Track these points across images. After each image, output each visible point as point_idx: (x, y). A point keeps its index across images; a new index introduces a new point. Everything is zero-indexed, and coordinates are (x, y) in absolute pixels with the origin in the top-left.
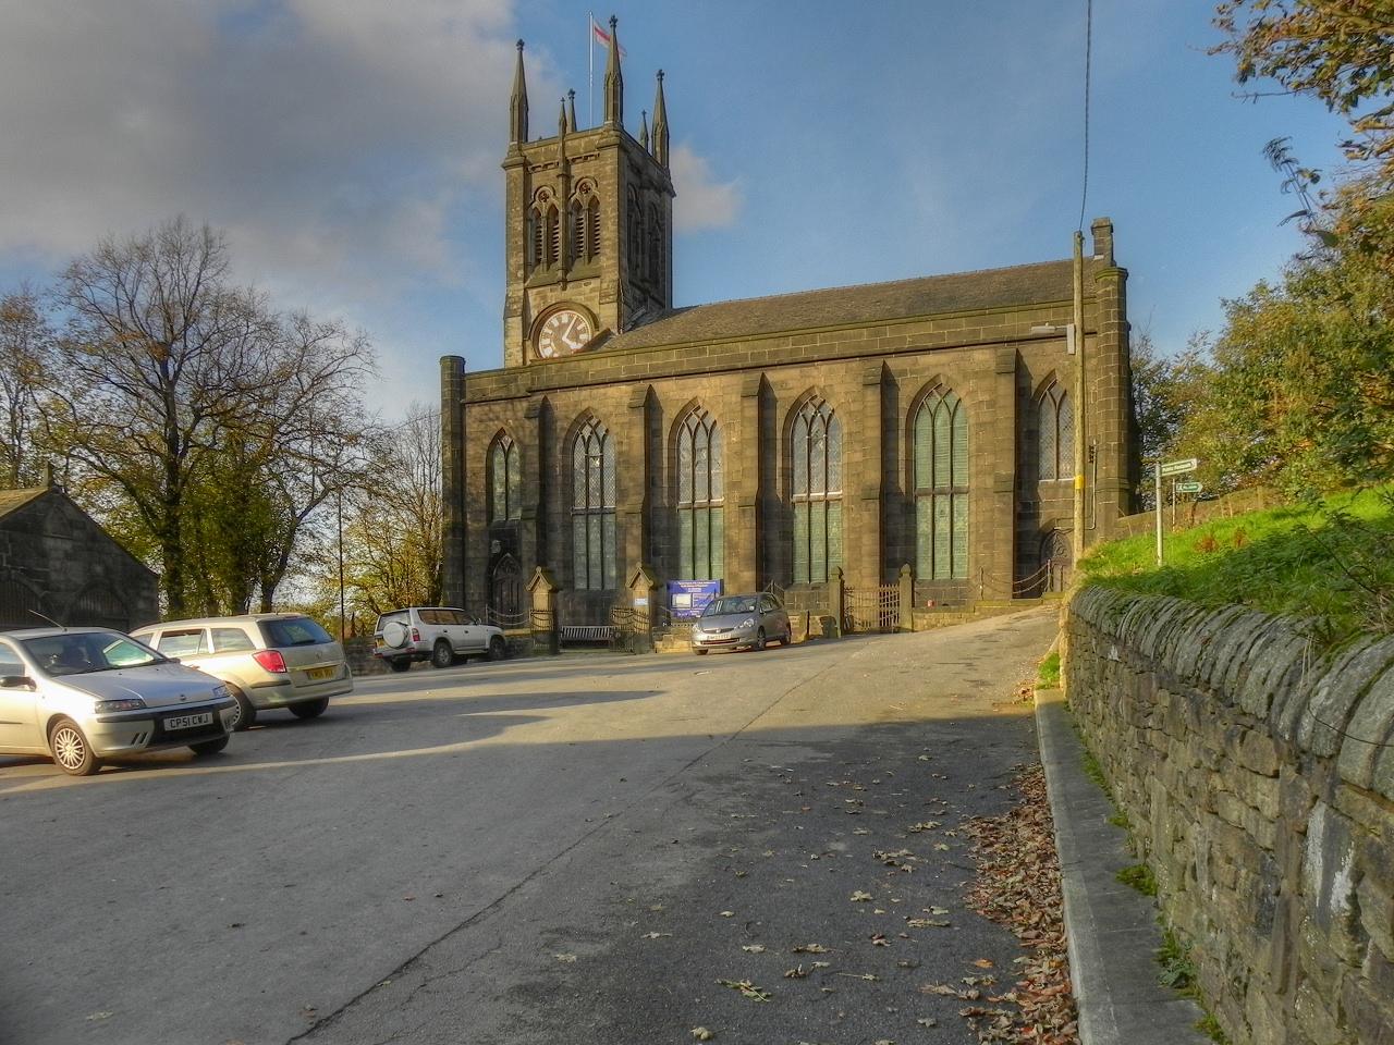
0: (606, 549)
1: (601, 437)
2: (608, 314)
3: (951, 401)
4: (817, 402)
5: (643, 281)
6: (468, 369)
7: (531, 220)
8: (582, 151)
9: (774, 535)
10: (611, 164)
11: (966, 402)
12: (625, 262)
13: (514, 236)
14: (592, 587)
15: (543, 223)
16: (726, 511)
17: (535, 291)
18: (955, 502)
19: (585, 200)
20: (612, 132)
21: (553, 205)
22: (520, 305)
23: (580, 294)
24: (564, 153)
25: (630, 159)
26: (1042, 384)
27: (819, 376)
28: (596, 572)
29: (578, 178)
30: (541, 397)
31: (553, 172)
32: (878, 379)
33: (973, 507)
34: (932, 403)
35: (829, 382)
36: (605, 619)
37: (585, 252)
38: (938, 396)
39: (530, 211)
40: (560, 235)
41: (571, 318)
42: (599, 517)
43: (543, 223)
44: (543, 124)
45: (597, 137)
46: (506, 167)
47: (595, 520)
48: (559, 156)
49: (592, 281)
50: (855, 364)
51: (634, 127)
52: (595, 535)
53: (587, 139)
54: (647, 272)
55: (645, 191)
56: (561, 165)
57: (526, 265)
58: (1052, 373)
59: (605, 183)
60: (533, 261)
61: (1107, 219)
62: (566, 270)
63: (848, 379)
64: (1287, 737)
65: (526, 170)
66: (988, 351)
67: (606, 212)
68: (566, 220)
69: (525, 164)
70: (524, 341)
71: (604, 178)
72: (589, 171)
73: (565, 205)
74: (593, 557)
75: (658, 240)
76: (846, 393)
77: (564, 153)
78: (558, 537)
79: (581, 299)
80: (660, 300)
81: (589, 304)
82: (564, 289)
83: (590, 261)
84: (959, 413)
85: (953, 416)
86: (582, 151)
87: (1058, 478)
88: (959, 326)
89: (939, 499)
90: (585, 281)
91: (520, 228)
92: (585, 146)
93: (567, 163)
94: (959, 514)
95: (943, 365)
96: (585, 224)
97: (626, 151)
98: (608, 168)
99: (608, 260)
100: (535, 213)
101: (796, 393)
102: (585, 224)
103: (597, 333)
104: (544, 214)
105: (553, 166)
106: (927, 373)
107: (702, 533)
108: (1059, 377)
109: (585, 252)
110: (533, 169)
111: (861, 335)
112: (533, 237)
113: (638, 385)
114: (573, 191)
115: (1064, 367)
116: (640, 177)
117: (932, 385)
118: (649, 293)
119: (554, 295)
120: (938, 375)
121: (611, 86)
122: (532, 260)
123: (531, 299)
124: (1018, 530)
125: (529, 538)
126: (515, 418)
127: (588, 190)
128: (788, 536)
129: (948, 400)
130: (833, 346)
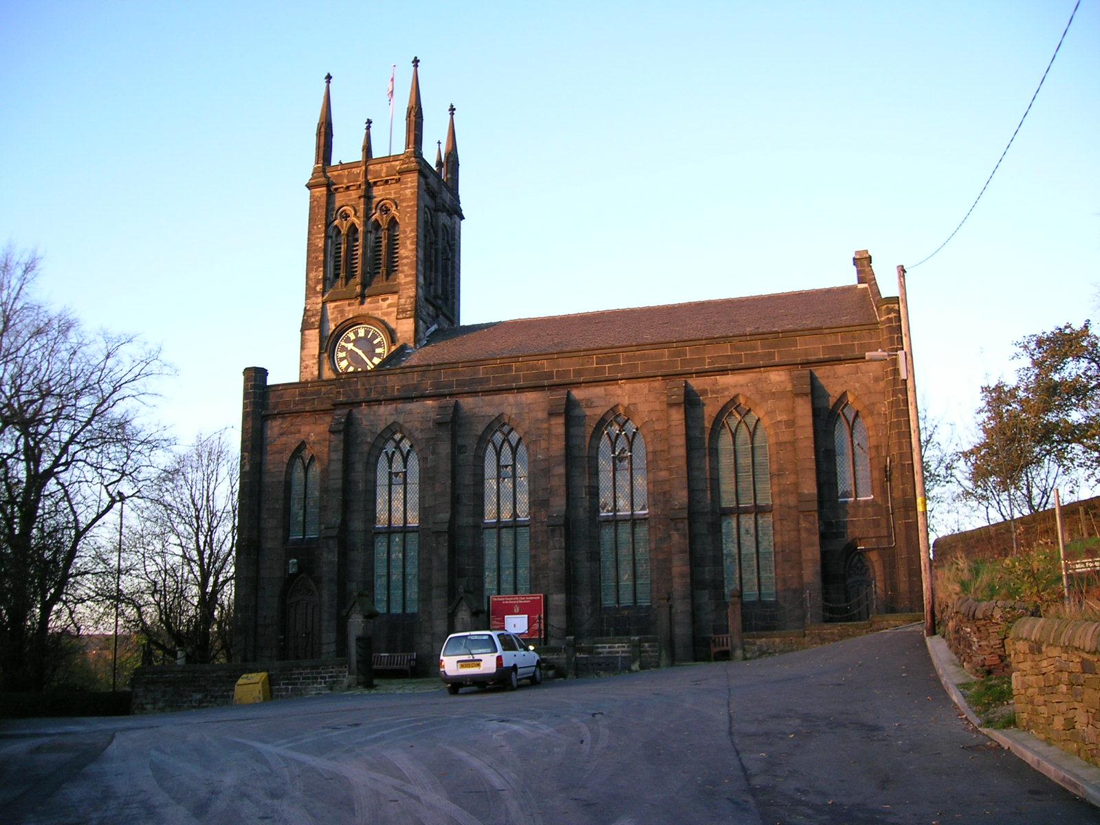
0: (408, 570)
1: (405, 453)
2: (406, 328)
3: (751, 420)
4: (621, 420)
5: (436, 297)
6: (270, 381)
7: (331, 237)
8: (383, 175)
9: (582, 555)
10: (411, 187)
11: (765, 422)
12: (421, 279)
13: (315, 251)
14: (393, 611)
15: (343, 239)
16: (532, 530)
17: (333, 305)
18: (760, 521)
19: (384, 221)
20: (413, 159)
21: (353, 225)
22: (318, 318)
23: (377, 309)
24: (366, 176)
25: (427, 184)
26: (837, 404)
27: (623, 394)
28: (397, 594)
29: (380, 199)
30: (346, 411)
31: (354, 194)
32: (682, 399)
33: (778, 527)
34: (733, 422)
35: (633, 401)
36: (409, 646)
37: (383, 269)
38: (738, 416)
39: (331, 228)
40: (360, 252)
41: (367, 332)
42: (401, 535)
43: (343, 239)
44: (346, 151)
45: (398, 163)
46: (309, 186)
47: (397, 539)
48: (361, 179)
49: (390, 297)
50: (657, 384)
51: (431, 158)
52: (397, 555)
53: (388, 164)
54: (440, 291)
55: (440, 213)
56: (363, 187)
57: (325, 279)
58: (844, 394)
59: (404, 205)
60: (332, 276)
61: (867, 251)
62: (365, 285)
63: (651, 398)
64: (672, 726)
65: (329, 190)
66: (782, 373)
67: (405, 232)
68: (365, 238)
69: (328, 185)
70: (320, 353)
71: (402, 201)
72: (390, 194)
73: (365, 224)
74: (394, 578)
75: (449, 259)
76: (650, 412)
77: (366, 176)
78: (358, 555)
79: (378, 314)
80: (451, 316)
81: (385, 318)
82: (362, 303)
83: (387, 279)
84: (759, 433)
85: (752, 435)
86: (383, 175)
87: (856, 497)
88: (754, 348)
89: (744, 519)
90: (383, 296)
91: (321, 244)
92: (387, 171)
93: (369, 186)
94: (764, 534)
95: (742, 386)
96: (384, 242)
97: (425, 177)
98: (408, 192)
99: (406, 277)
100: (336, 230)
101: (600, 412)
102: (384, 242)
103: (393, 348)
104: (344, 231)
105: (355, 188)
106: (726, 393)
107: (508, 554)
108: (850, 398)
109: (383, 269)
110: (336, 189)
111: (662, 355)
112: (333, 253)
113: (444, 401)
114: (374, 211)
115: (856, 389)
116: (435, 200)
117: (732, 405)
118: (441, 309)
119: (351, 310)
120: (739, 394)
121: (413, 118)
122: (330, 274)
123: (329, 312)
124: (243, 481)
125: (329, 557)
126: (315, 432)
127: (387, 210)
128: (595, 556)
129: (748, 419)
130: (636, 366)
